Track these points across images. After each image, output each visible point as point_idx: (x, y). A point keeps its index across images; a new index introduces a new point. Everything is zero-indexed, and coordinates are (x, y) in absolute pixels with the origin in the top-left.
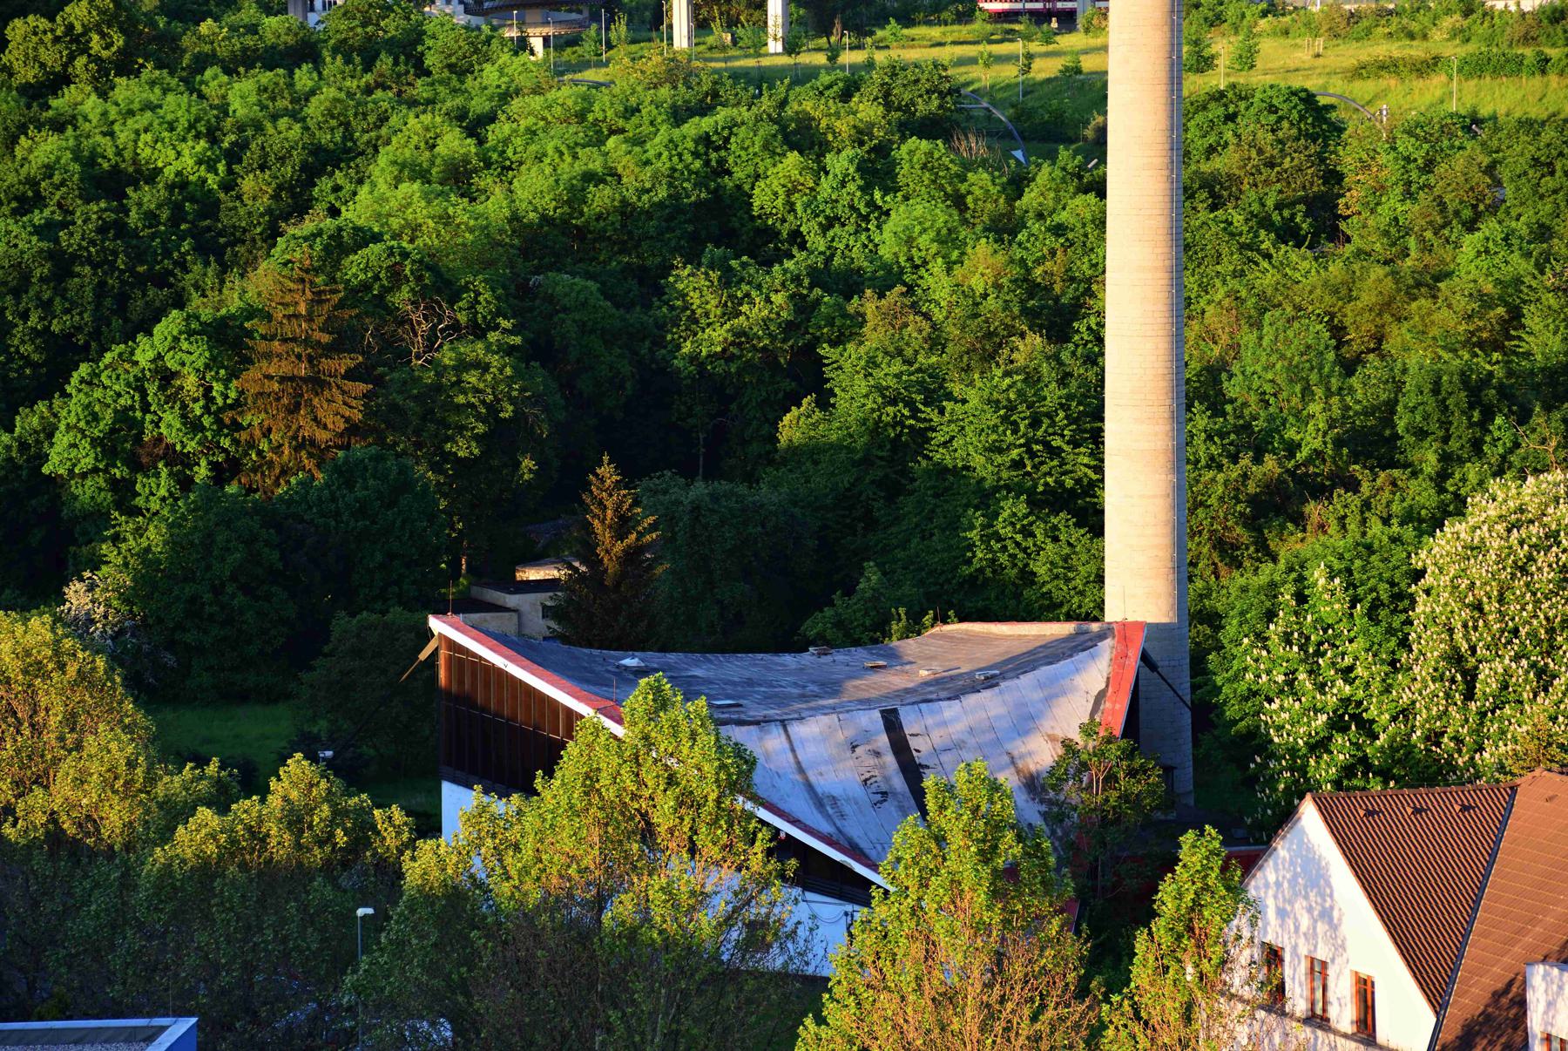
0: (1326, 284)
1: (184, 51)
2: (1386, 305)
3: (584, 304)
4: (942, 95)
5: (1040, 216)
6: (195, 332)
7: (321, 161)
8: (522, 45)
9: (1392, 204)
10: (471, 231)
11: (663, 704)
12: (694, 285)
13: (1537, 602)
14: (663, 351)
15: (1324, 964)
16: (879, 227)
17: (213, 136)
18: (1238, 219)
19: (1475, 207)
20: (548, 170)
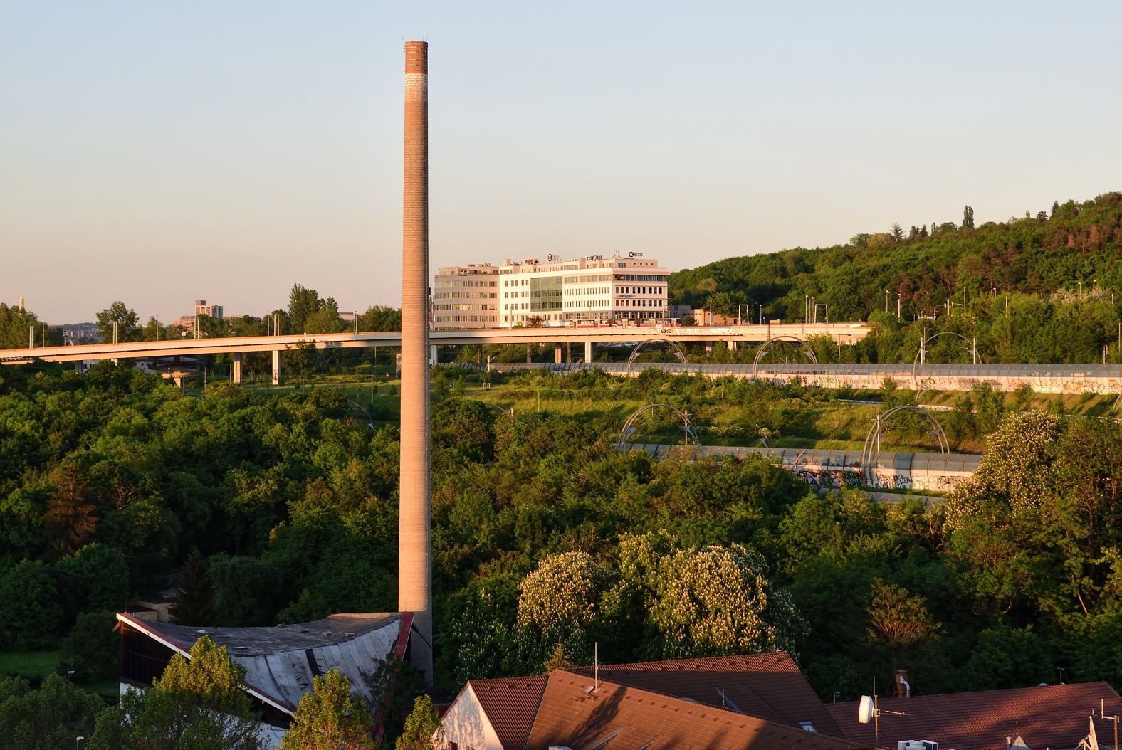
0: (489, 477)
1: (29, 384)
2: (512, 486)
4: (340, 401)
5: (378, 449)
6: (26, 498)
7: (83, 427)
8: (171, 381)
9: (514, 447)
10: (144, 455)
11: (208, 648)
12: (238, 477)
13: (564, 603)
16: (313, 453)
17: (39, 418)
18: (455, 452)
19: (545, 449)
20: (177, 430)
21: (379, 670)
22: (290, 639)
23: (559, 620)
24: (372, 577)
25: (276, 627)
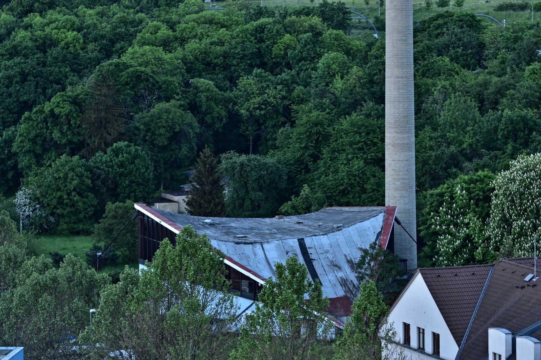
3: (208, 90)
13: (533, 200)
14: (237, 107)
15: (423, 330)
21: (363, 258)
22: (285, 229)
23: (528, 214)
24: (366, 175)
25: (274, 219)
